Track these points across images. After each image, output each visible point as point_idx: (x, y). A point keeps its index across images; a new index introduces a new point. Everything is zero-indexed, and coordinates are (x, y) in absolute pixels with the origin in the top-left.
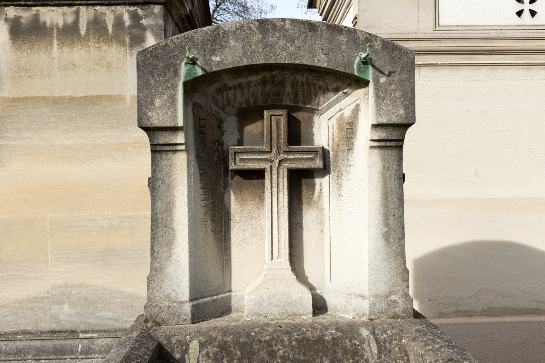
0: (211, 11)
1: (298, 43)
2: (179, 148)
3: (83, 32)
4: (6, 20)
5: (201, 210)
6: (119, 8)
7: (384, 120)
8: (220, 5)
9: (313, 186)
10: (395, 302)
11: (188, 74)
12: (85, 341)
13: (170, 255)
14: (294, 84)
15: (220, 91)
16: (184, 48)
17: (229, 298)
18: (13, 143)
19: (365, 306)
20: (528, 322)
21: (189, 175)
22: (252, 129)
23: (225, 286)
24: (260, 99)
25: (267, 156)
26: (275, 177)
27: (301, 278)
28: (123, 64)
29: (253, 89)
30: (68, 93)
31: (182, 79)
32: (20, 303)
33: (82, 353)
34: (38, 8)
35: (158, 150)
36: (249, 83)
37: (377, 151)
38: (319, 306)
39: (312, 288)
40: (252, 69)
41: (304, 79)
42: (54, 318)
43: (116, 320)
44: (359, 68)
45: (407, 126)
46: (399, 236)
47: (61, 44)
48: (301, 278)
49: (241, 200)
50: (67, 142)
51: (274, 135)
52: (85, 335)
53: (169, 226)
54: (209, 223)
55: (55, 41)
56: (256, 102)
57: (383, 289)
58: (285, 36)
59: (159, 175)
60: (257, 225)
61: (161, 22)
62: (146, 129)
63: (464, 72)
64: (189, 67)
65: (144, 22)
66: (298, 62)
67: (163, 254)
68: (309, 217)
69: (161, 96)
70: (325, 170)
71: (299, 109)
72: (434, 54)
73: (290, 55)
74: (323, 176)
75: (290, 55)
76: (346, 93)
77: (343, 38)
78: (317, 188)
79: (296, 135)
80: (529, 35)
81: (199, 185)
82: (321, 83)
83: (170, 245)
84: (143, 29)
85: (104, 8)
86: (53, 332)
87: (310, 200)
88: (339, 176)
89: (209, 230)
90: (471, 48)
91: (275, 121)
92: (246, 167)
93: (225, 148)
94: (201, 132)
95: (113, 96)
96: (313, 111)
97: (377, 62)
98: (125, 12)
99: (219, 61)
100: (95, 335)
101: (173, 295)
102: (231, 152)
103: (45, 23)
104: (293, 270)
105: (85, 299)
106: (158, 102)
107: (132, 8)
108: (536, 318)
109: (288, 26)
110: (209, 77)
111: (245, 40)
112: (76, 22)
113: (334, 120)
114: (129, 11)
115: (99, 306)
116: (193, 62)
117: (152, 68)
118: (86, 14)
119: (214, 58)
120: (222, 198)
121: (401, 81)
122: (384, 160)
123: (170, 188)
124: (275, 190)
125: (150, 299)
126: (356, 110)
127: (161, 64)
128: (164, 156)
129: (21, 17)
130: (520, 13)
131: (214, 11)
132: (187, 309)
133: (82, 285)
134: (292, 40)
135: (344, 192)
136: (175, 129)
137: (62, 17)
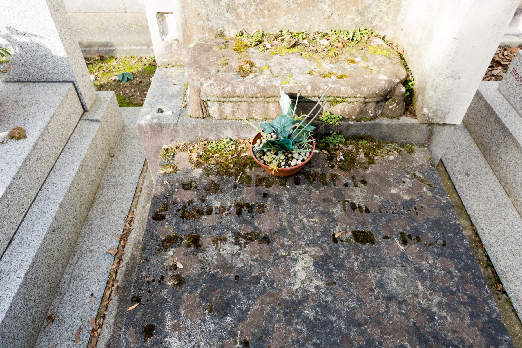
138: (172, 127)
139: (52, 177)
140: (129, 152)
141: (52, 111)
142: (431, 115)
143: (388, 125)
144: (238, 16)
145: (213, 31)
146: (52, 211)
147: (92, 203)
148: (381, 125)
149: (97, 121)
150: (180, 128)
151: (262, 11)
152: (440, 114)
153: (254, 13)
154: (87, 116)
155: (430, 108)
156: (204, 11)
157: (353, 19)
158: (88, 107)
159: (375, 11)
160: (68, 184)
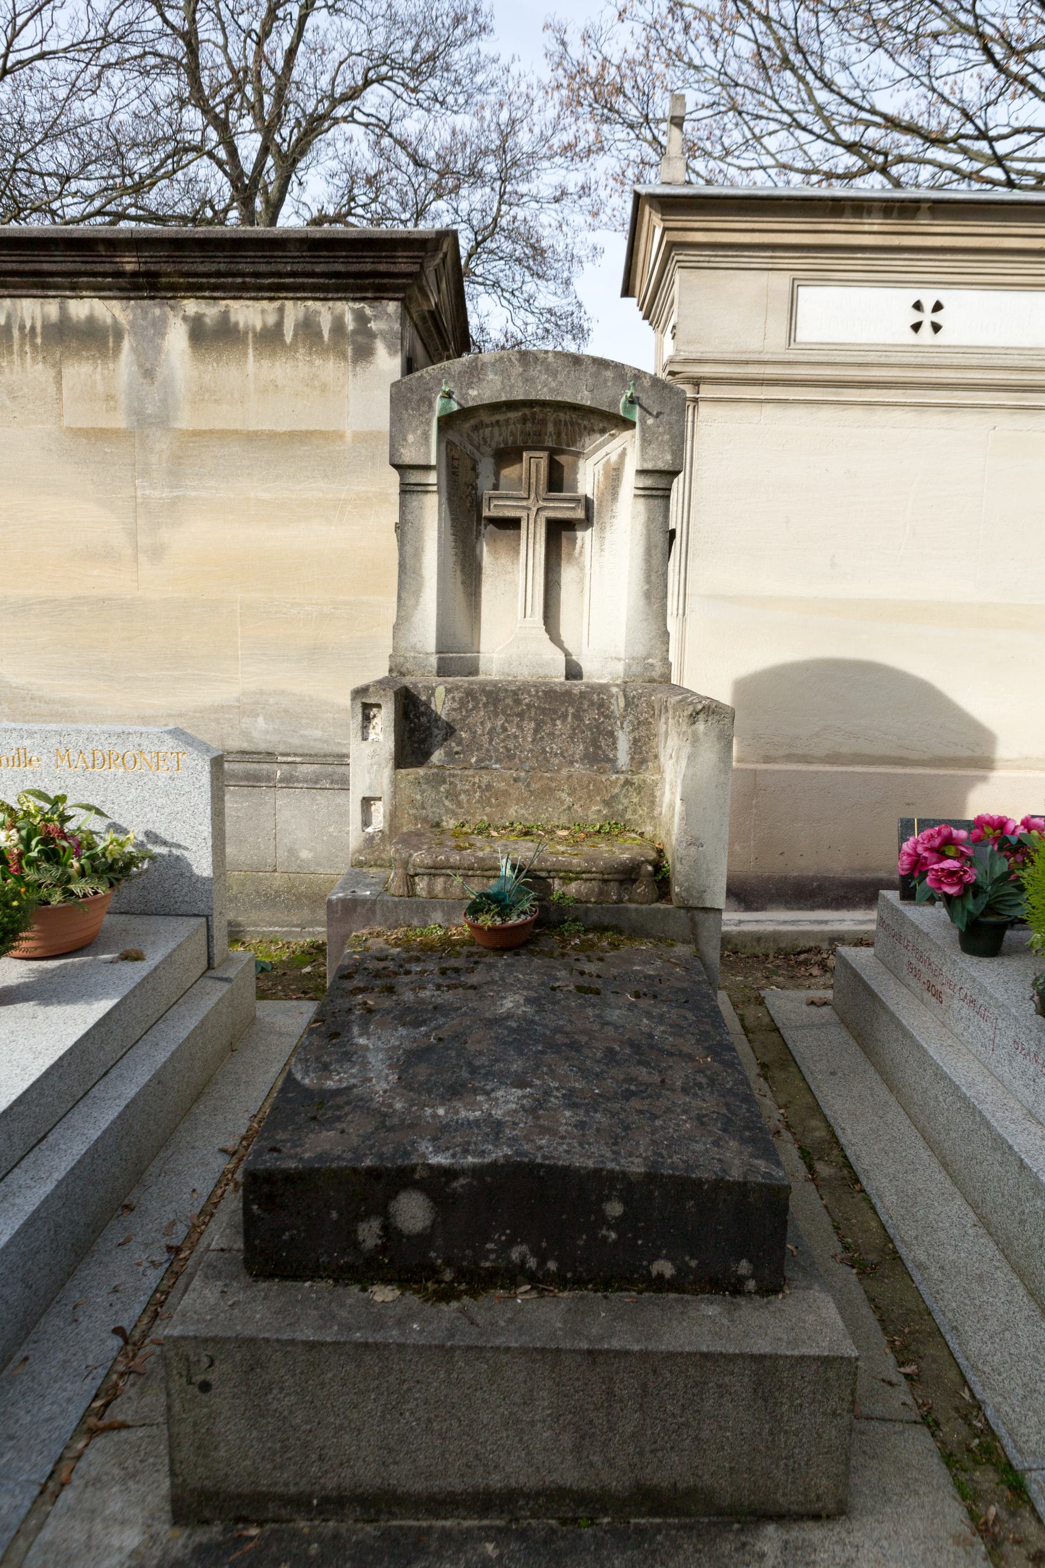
0: (463, 253)
1: (560, 378)
2: (431, 488)
3: (288, 339)
4: (185, 318)
5: (451, 559)
6: (339, 304)
7: (649, 466)
8: (484, 240)
9: (574, 541)
10: (652, 665)
11: (442, 409)
12: (284, 766)
13: (417, 603)
14: (557, 423)
15: (475, 428)
16: (440, 380)
17: (477, 659)
18: (194, 494)
19: (620, 668)
20: (886, 774)
21: (440, 519)
22: (509, 473)
23: (474, 645)
24: (519, 438)
25: (524, 503)
26: (531, 527)
27: (555, 638)
28: (343, 386)
29: (511, 427)
30: (267, 426)
31: (437, 414)
32: (201, 712)
33: (281, 781)
34: (228, 302)
35: (407, 490)
36: (507, 421)
37: (642, 500)
38: (573, 672)
39: (567, 654)
40: (511, 405)
41: (568, 417)
42: (245, 734)
43: (326, 741)
44: (625, 408)
45: (676, 473)
46: (661, 595)
47: (259, 355)
48: (555, 638)
49: (494, 552)
50: (266, 496)
51: (533, 480)
52: (285, 759)
53: (417, 572)
54: (458, 573)
55: (250, 351)
56: (515, 442)
57: (640, 650)
58: (547, 370)
59: (409, 517)
60: (511, 578)
61: (397, 326)
62: (396, 466)
63: (826, 412)
64: (445, 400)
65: (373, 325)
66: (559, 399)
67: (410, 602)
68: (568, 574)
69: (414, 432)
70: (588, 521)
71: (562, 452)
72: (784, 385)
73: (551, 390)
74: (586, 529)
75: (551, 390)
76: (613, 435)
77: (609, 374)
78: (579, 542)
79: (557, 480)
80: (925, 361)
81: (450, 531)
82: (586, 423)
83: (417, 593)
84: (372, 335)
85: (319, 304)
86: (244, 752)
87: (570, 555)
88: (602, 529)
89: (459, 581)
90: (838, 378)
91: (534, 464)
92: (501, 514)
93: (479, 493)
94: (454, 473)
95: (328, 432)
96: (578, 455)
97: (645, 402)
98: (346, 310)
99: (477, 395)
100: (298, 759)
101: (419, 645)
102: (486, 497)
103: (237, 324)
104: (547, 630)
105: (286, 711)
106: (411, 438)
107: (357, 305)
108: (899, 770)
109: (551, 358)
110: (466, 412)
111: (505, 373)
112: (280, 324)
113: (600, 466)
114: (352, 310)
115: (304, 721)
116: (449, 395)
117: (404, 401)
118: (294, 311)
119: (470, 392)
120: (474, 549)
121: (670, 423)
122: (650, 511)
123: (419, 531)
124: (531, 541)
125: (395, 649)
126: (623, 455)
127: (415, 397)
128: (414, 497)
129: (204, 315)
130: (916, 327)
131: (470, 256)
132: (433, 660)
133: (283, 692)
134: (555, 374)
135: (606, 547)
136: (427, 468)
137: (260, 316)
138: (368, 906)
139: (161, 1025)
140: (262, 1048)
141: (179, 940)
142: (684, 894)
143: (636, 909)
144: (459, 805)
145: (427, 822)
146: (161, 1057)
147: (197, 1097)
148: (627, 910)
149: (227, 980)
150: (378, 906)
151: (489, 799)
152: (695, 893)
153: (478, 802)
154: (210, 973)
155: (681, 886)
156: (418, 797)
157: (599, 811)
158: (217, 961)
159: (625, 801)
160: (185, 1034)
